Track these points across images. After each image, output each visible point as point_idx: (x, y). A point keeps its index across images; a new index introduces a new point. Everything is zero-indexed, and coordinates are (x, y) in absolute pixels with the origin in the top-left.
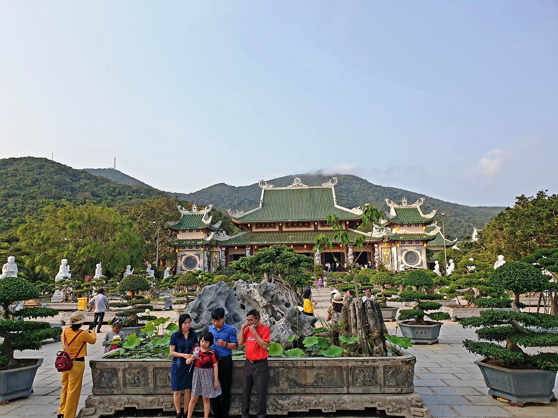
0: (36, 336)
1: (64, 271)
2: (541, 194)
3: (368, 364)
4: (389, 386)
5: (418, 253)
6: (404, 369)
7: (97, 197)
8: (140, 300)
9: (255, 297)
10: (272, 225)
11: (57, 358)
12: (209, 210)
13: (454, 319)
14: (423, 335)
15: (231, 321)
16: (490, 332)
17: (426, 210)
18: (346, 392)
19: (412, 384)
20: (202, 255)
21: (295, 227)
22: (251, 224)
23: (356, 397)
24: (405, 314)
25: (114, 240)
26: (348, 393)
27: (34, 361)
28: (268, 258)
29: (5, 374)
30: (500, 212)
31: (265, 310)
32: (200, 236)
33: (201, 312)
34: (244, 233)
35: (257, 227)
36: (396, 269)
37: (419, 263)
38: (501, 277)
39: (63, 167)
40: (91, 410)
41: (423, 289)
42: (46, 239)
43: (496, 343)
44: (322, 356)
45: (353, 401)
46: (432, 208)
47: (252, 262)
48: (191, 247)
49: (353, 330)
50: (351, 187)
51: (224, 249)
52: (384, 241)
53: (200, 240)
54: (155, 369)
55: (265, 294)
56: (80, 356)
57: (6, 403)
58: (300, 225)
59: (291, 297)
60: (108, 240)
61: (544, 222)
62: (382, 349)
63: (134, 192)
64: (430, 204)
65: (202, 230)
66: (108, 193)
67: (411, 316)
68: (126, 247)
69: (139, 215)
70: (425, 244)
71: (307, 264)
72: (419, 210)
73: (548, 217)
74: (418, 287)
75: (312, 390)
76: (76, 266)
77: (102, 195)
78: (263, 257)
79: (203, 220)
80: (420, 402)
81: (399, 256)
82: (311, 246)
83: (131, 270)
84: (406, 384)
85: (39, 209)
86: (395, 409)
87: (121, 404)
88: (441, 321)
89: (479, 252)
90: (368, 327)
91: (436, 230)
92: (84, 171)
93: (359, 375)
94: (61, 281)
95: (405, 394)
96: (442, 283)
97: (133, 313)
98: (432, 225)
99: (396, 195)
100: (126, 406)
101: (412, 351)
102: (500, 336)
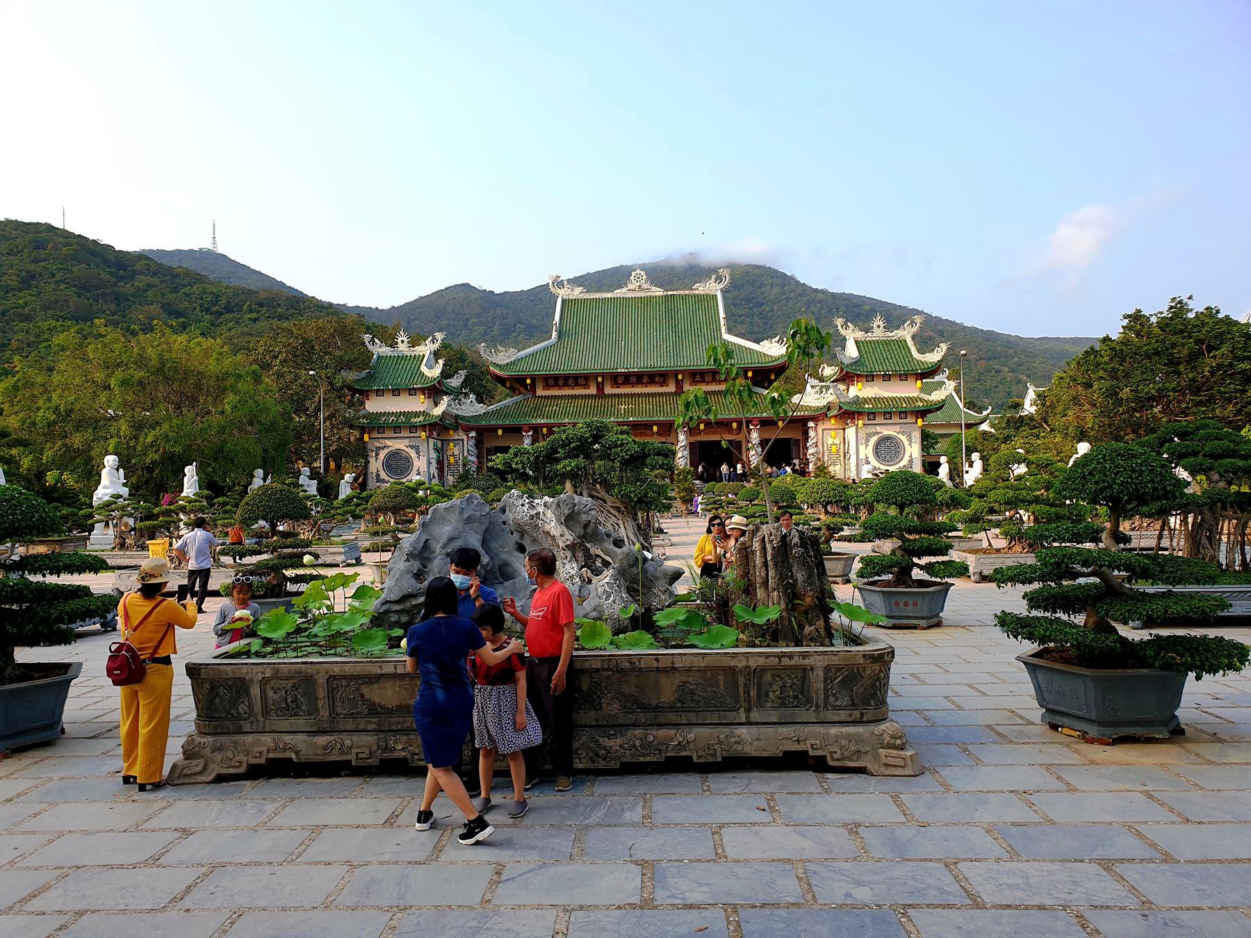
0: (65, 615)
1: (112, 483)
2: (1179, 308)
3: (793, 662)
4: (836, 708)
5: (904, 439)
9: (547, 527)
10: (582, 381)
11: (110, 657)
12: (437, 346)
13: (977, 577)
15: (497, 578)
16: (1053, 596)
17: (925, 344)
18: (744, 720)
19: (883, 702)
20: (423, 447)
22: (533, 379)
23: (763, 729)
24: (872, 566)
25: (223, 413)
26: (748, 723)
27: (63, 668)
30: (1087, 348)
31: (569, 554)
32: (418, 404)
33: (429, 559)
34: (517, 398)
36: (853, 475)
38: (1084, 477)
39: (91, 245)
40: (197, 765)
41: (915, 516)
43: (1064, 617)
45: (758, 739)
46: (938, 339)
47: (537, 458)
48: (397, 428)
49: (760, 593)
50: (760, 293)
51: (473, 434)
52: (830, 414)
53: (417, 414)
55: (569, 520)
56: (161, 653)
58: (645, 380)
59: (625, 530)
61: (1181, 368)
62: (822, 631)
63: (261, 305)
64: (935, 330)
65: (423, 390)
67: (885, 569)
68: (249, 428)
70: (920, 421)
71: (660, 460)
72: (910, 343)
73: (1193, 358)
74: (901, 507)
75: (672, 717)
78: (563, 446)
79: (424, 369)
80: (900, 738)
81: (862, 448)
85: (43, 345)
86: (846, 754)
88: (950, 580)
89: (1037, 437)
90: (794, 585)
91: (945, 389)
92: (142, 256)
93: (770, 685)
94: (107, 505)
95: (868, 722)
96: (955, 503)
97: (275, 568)
98: (937, 378)
99: (860, 310)
100: (272, 755)
102: (1070, 602)
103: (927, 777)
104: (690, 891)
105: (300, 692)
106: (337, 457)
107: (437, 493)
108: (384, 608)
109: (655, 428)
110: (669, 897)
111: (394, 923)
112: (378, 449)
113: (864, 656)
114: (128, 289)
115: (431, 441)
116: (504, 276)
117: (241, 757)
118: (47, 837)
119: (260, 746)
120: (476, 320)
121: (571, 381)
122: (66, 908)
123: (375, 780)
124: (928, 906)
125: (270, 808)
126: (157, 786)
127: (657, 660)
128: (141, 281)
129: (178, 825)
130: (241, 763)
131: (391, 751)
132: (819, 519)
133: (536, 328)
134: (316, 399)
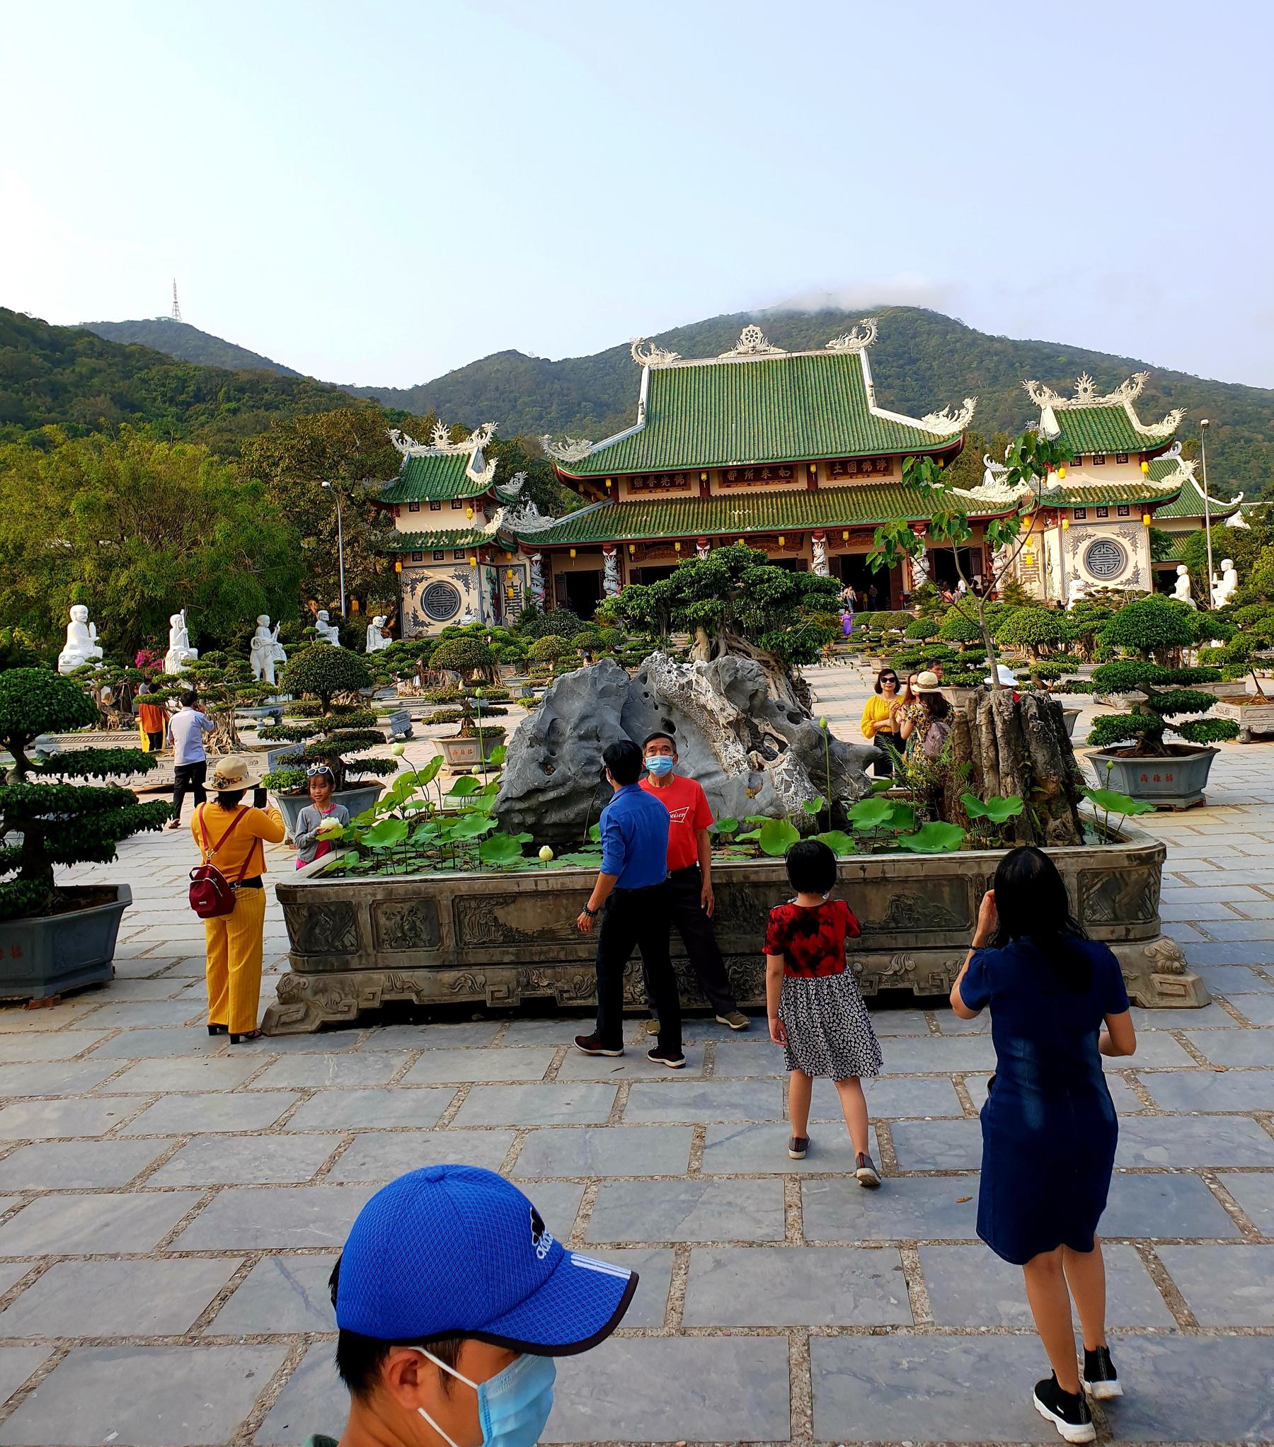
0: (102, 824)
1: (82, 642)
6: (1134, 877)
7: (133, 412)
8: (347, 718)
9: (702, 700)
10: (680, 480)
12: (486, 441)
14: (1163, 783)
17: (1150, 408)
19: (1154, 914)
20: (473, 578)
21: (749, 482)
22: (615, 480)
28: (706, 585)
29: (47, 925)
31: (732, 733)
32: (461, 520)
33: (557, 744)
35: (633, 489)
37: (1128, 574)
39: (17, 322)
40: (296, 1011)
42: (15, 548)
44: (909, 850)
46: (1164, 400)
48: (438, 553)
49: (988, 779)
50: (920, 350)
51: (537, 557)
52: (1022, 512)
53: (464, 534)
54: (458, 899)
55: (731, 690)
56: (250, 875)
57: (57, 1002)
58: (765, 475)
60: (195, 543)
62: (1070, 826)
63: (242, 390)
64: (1164, 390)
65: (470, 501)
66: (164, 395)
68: (248, 561)
69: (276, 464)
70: (1147, 517)
71: (822, 599)
72: (1130, 411)
75: (885, 941)
76: (110, 625)
77: (147, 403)
78: (692, 584)
79: (470, 472)
80: (1178, 959)
82: (799, 539)
83: (272, 628)
84: (1140, 914)
87: (374, 994)
88: (1215, 745)
90: (1032, 769)
92: (83, 332)
95: (1136, 940)
96: (1206, 634)
97: (330, 755)
98: (1166, 456)
100: (387, 997)
101: (1150, 828)
103: (1215, 1011)
104: (941, 1154)
105: (419, 917)
106: (360, 594)
107: (501, 640)
108: (505, 806)
109: (782, 540)
110: (917, 1162)
111: (590, 1196)
112: (415, 581)
113: (1129, 856)
114: (66, 376)
115: (484, 569)
116: (563, 337)
117: (350, 1000)
118: (144, 1100)
119: (374, 986)
120: (526, 399)
121: (664, 482)
122: (200, 1182)
123: (516, 1025)
124: (1242, 1169)
125: (398, 1062)
126: (252, 1037)
127: (863, 869)
128: (84, 364)
129: (294, 1084)
130: (349, 1007)
131: (534, 988)
132: (1026, 665)
133: (608, 405)
134: (332, 519)
